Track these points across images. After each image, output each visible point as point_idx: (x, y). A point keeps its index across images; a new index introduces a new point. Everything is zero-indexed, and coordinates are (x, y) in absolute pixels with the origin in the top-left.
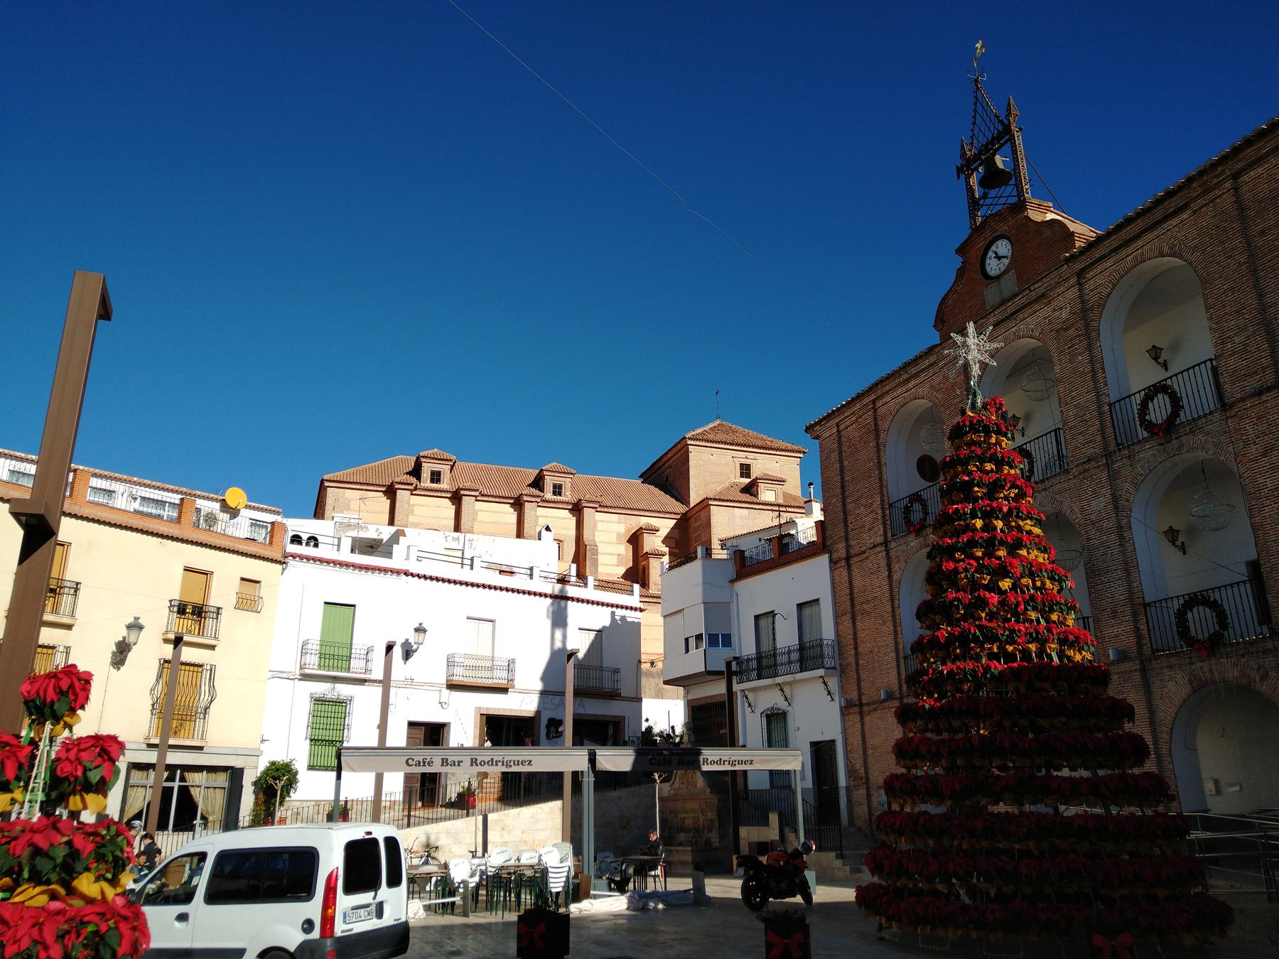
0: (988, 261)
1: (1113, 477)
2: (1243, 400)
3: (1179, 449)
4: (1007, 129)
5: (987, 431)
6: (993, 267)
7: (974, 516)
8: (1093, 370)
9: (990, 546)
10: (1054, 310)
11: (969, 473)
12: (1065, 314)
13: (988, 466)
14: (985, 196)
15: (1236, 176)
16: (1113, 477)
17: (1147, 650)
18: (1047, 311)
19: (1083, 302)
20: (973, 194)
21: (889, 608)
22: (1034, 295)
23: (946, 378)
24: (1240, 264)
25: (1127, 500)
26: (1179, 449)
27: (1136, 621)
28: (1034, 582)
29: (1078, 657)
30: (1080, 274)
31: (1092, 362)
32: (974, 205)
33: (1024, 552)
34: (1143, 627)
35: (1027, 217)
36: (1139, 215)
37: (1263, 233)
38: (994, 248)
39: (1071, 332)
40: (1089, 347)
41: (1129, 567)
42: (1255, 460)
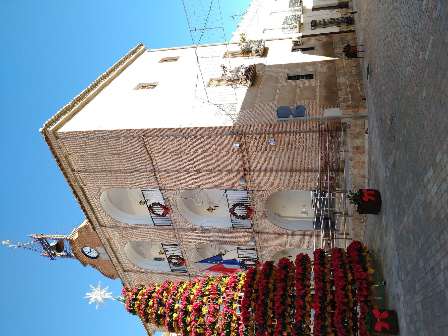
0: (91, 256)
1: (183, 229)
2: (158, 183)
3: (175, 206)
4: (39, 239)
5: (135, 299)
6: (94, 254)
7: (171, 317)
8: (140, 228)
9: (186, 313)
10: (114, 237)
11: (151, 314)
13: (151, 303)
14: (66, 251)
15: (73, 171)
17: (251, 230)
18: (115, 240)
19: (113, 227)
20: (63, 255)
22: (107, 243)
23: (136, 279)
24: (107, 175)
25: (193, 226)
26: (175, 206)
27: (239, 232)
28: (206, 295)
29: (242, 282)
30: (101, 226)
31: (137, 228)
32: (68, 256)
33: (192, 297)
34: (242, 230)
35: (76, 240)
36: (81, 203)
37: (97, 166)
38: (86, 253)
39: (124, 233)
40: (131, 228)
41: (219, 230)
42: (181, 184)
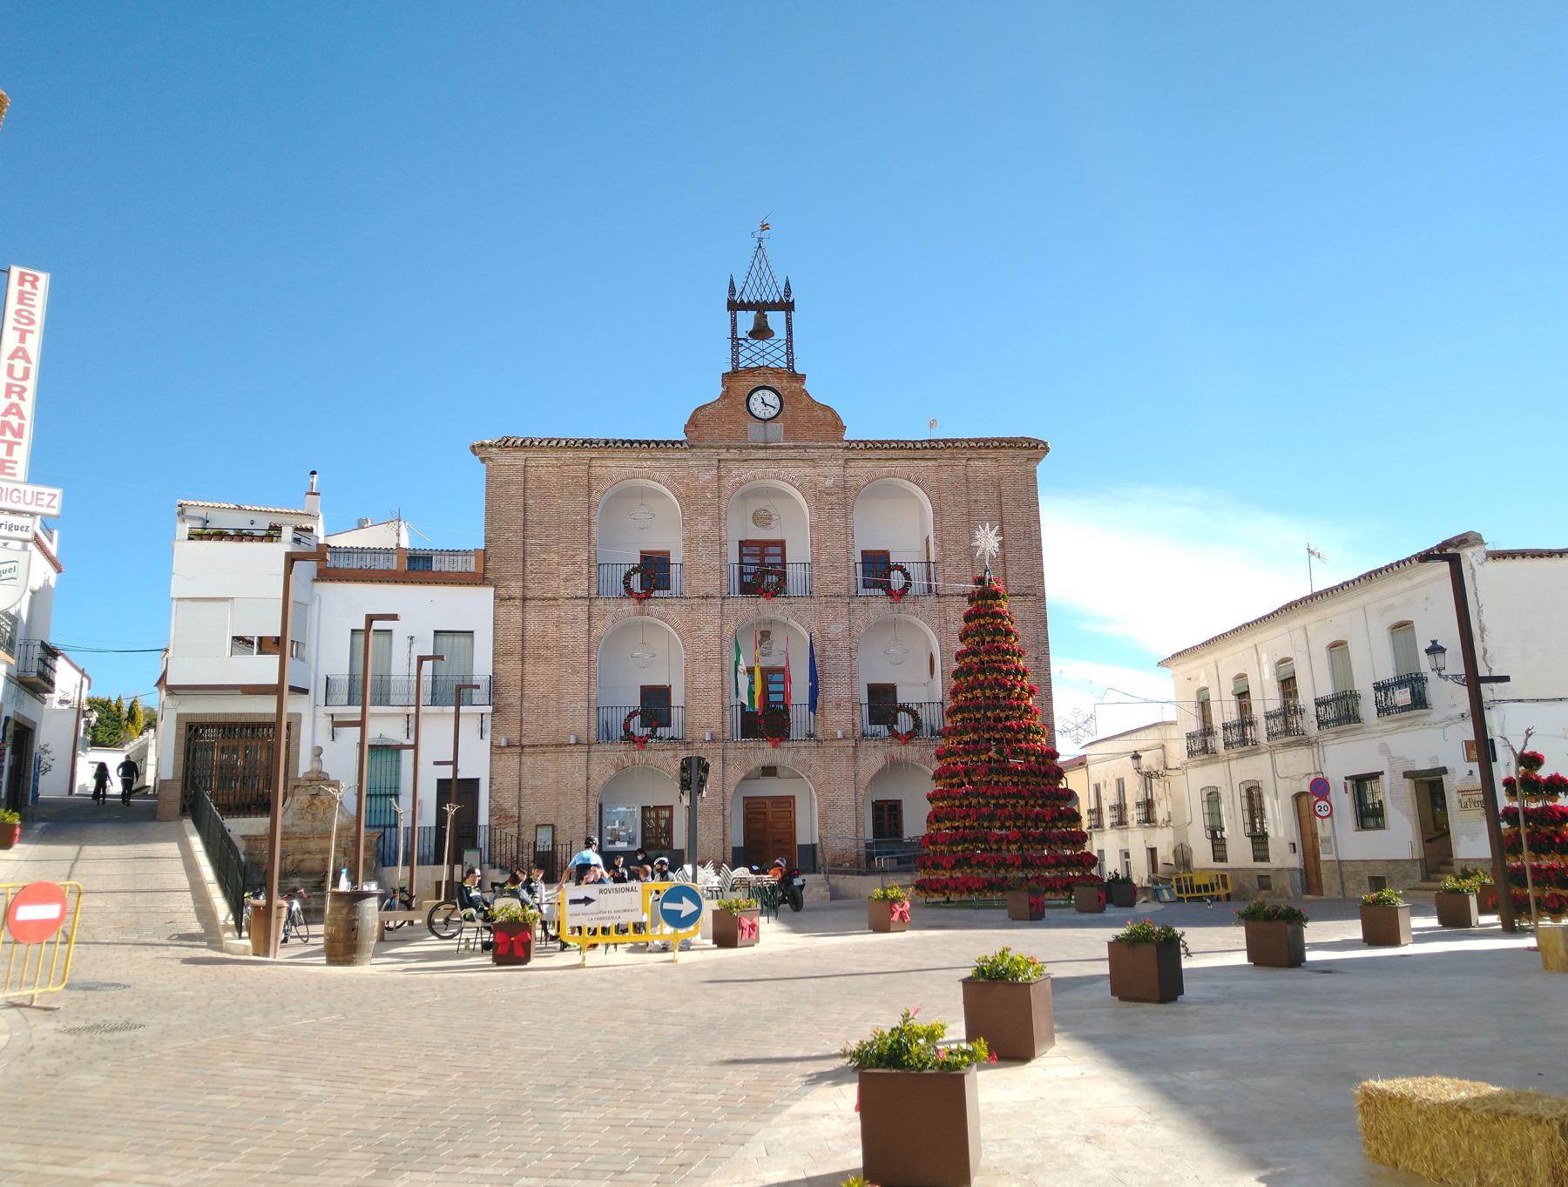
12: (829, 483)
16: (851, 612)
21: (585, 660)
